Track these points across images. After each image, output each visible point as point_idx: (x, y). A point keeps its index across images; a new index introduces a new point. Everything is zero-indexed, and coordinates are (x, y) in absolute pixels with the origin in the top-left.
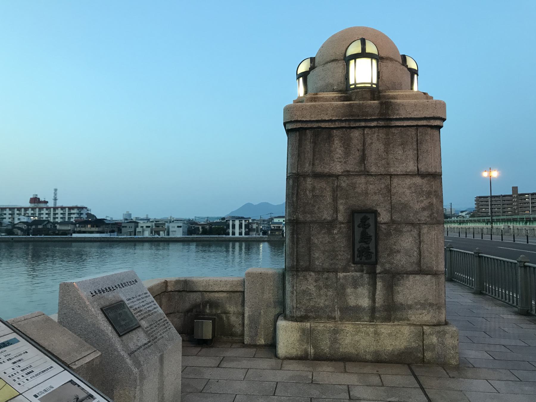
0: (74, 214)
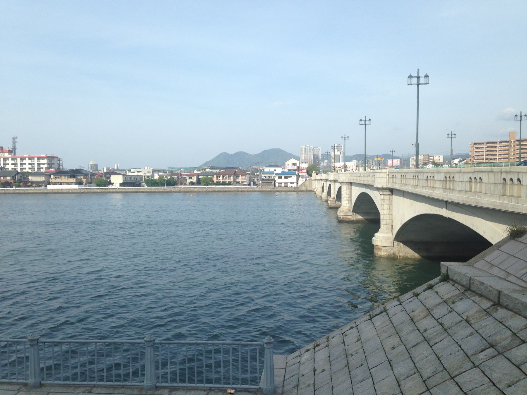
0: (44, 164)
